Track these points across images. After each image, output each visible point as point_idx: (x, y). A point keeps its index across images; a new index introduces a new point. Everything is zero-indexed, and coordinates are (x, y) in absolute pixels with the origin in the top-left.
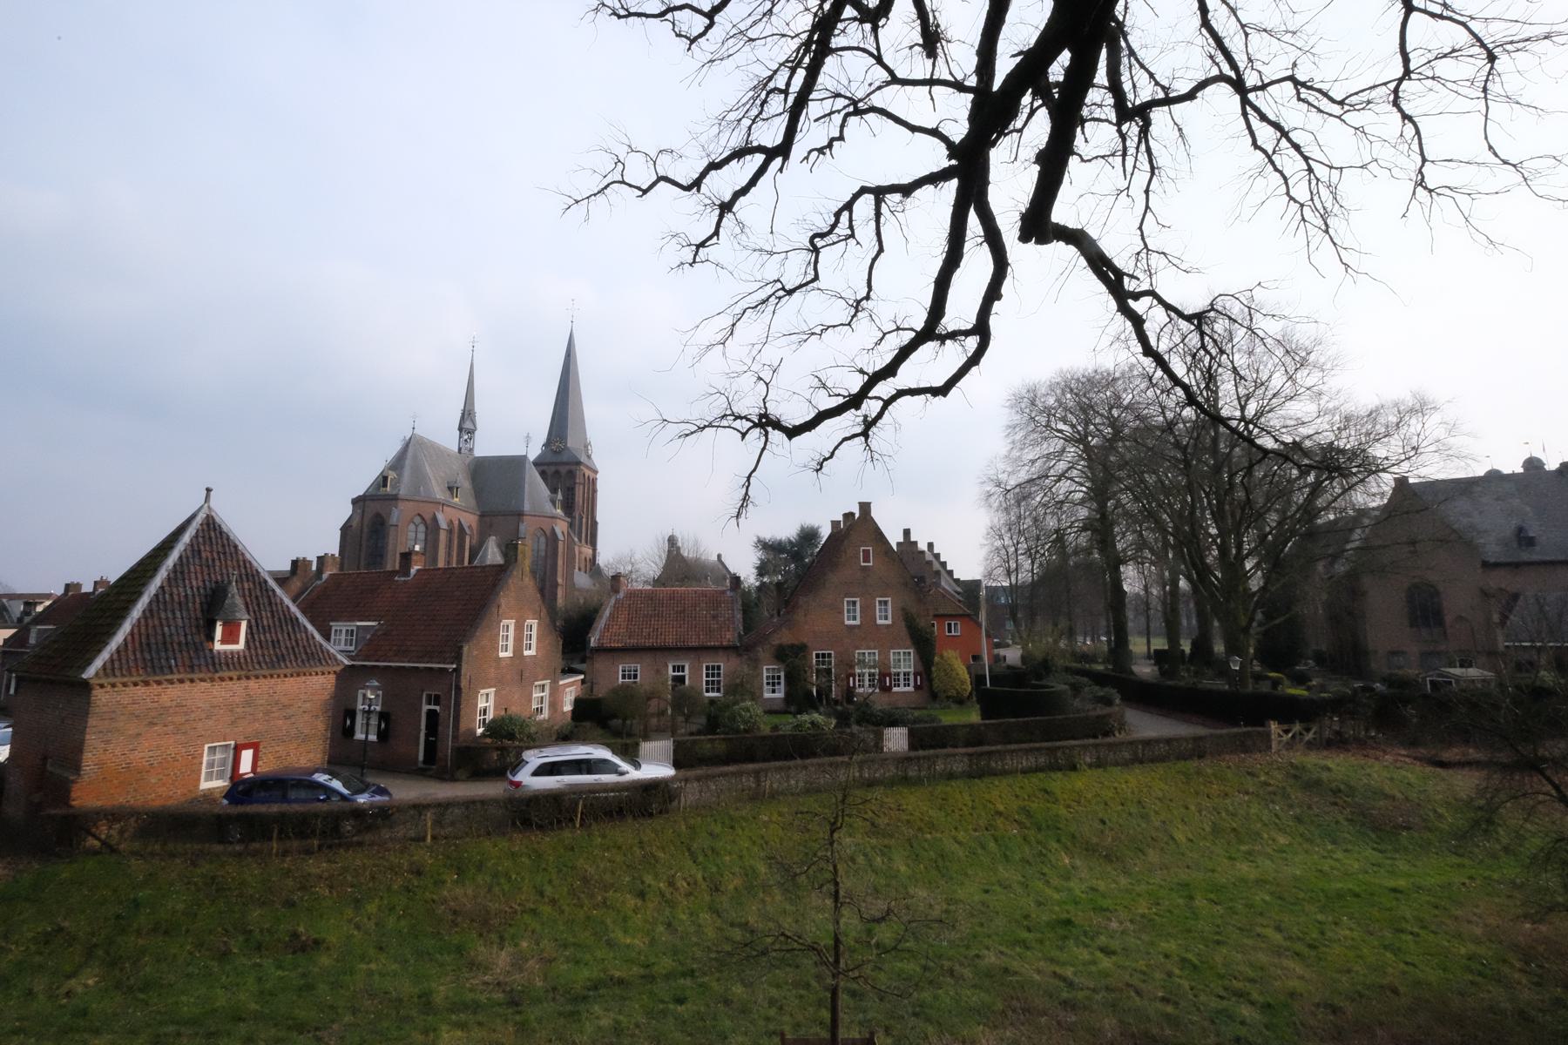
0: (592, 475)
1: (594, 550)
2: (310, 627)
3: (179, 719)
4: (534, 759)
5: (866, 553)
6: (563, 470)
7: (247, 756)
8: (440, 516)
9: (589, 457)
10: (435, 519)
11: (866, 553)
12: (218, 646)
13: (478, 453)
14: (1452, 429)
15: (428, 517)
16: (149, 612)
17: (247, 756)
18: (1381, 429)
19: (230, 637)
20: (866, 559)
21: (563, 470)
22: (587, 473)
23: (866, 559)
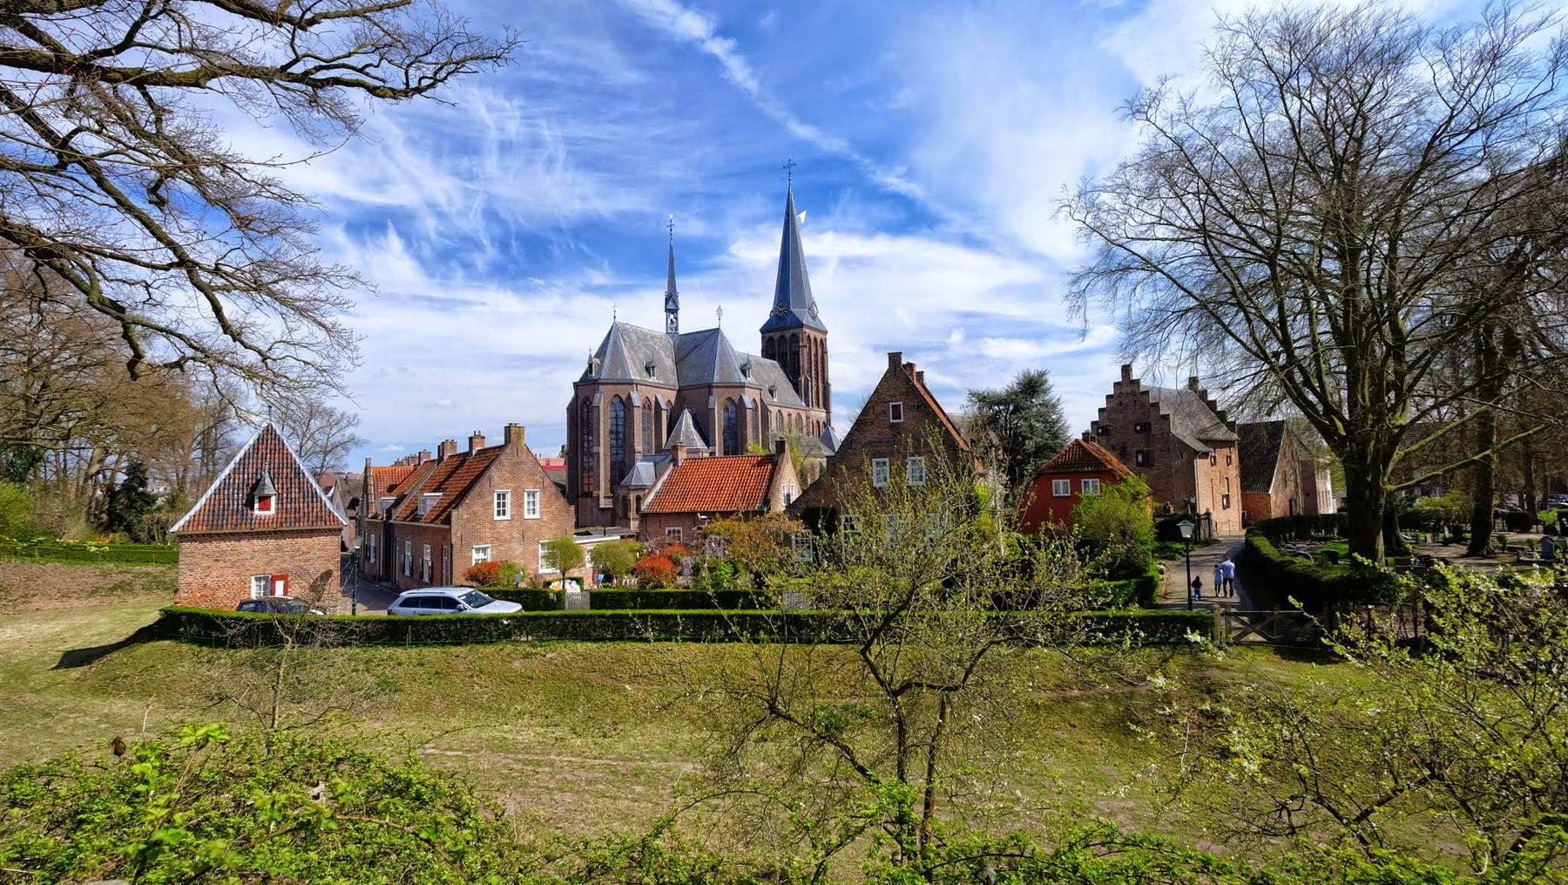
0: (819, 336)
1: (828, 412)
2: (203, 501)
3: (234, 558)
4: (405, 594)
5: (896, 408)
6: (788, 334)
7: (279, 585)
8: (634, 395)
9: (814, 318)
10: (629, 397)
11: (896, 408)
12: (257, 512)
13: (681, 332)
14: (1283, 83)
15: (624, 397)
16: (218, 491)
17: (279, 585)
18: (1361, 94)
19: (265, 506)
20: (897, 416)
21: (788, 334)
22: (813, 334)
23: (897, 416)
